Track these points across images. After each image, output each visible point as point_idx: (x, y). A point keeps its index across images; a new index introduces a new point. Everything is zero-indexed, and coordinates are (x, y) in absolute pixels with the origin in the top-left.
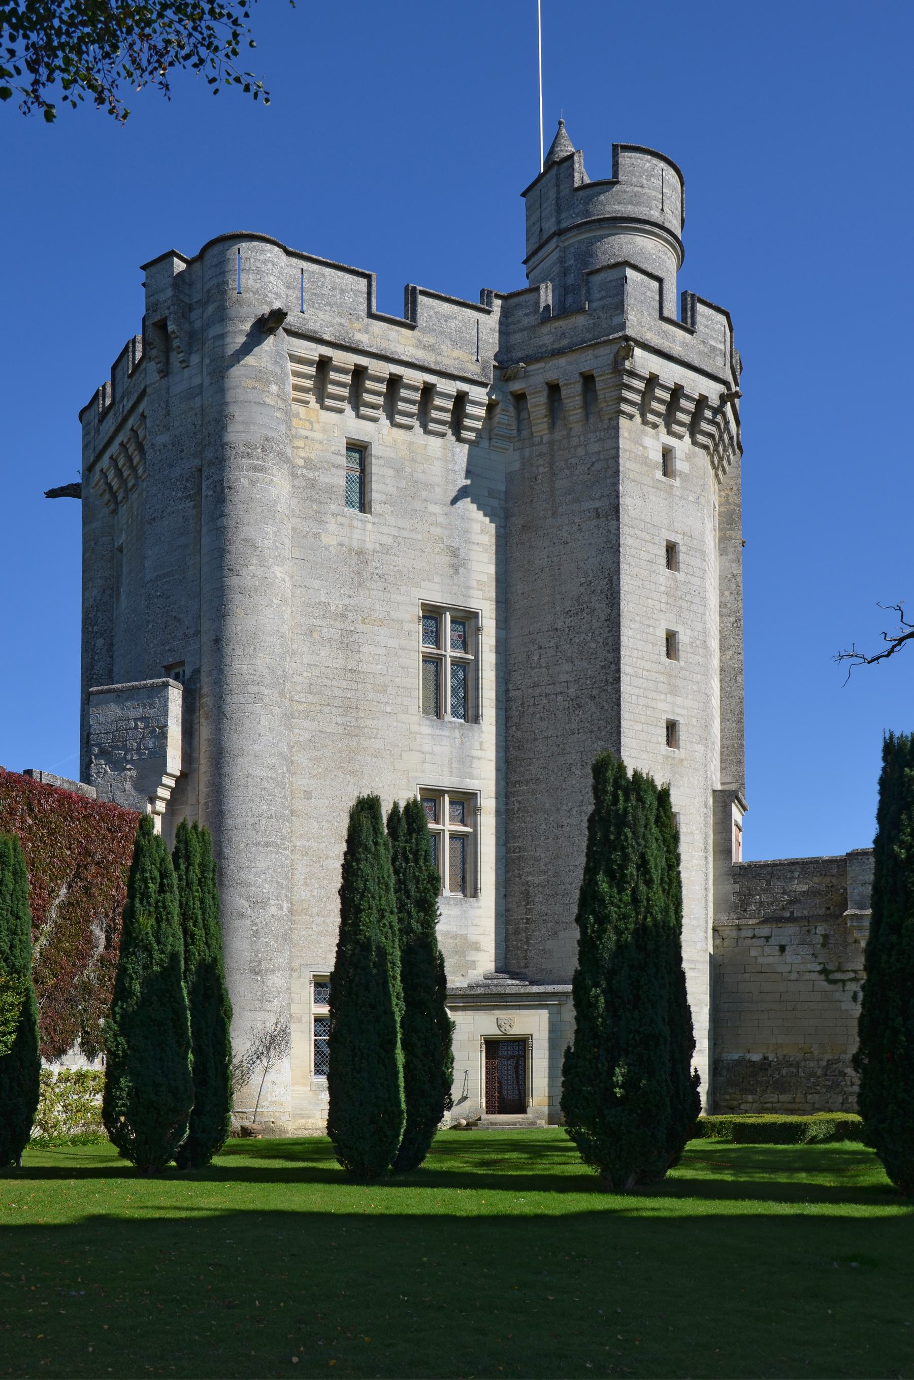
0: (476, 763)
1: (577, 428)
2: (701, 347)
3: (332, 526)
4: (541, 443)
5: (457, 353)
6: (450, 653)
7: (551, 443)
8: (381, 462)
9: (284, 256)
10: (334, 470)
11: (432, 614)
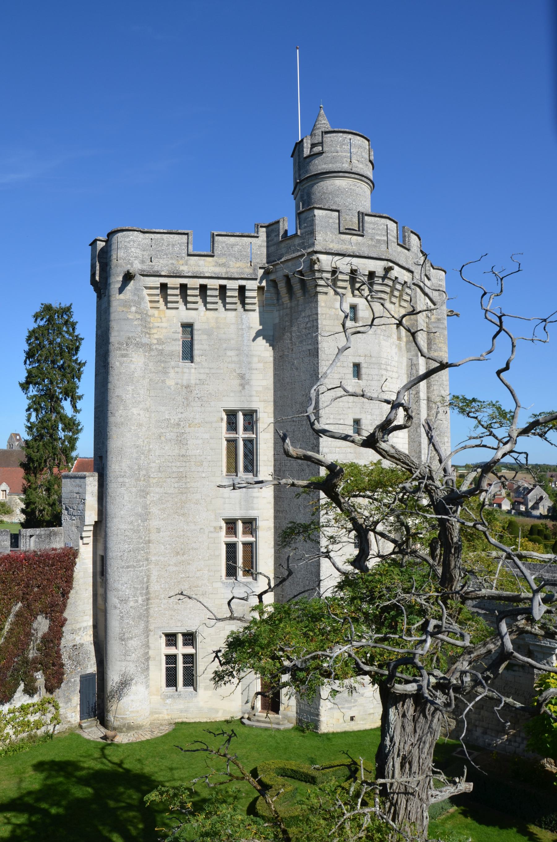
0: (255, 501)
1: (301, 299)
2: (370, 242)
3: (172, 374)
4: (287, 308)
5: (239, 264)
6: (241, 434)
7: (291, 308)
8: (200, 332)
9: (141, 235)
10: (173, 342)
11: (231, 415)
